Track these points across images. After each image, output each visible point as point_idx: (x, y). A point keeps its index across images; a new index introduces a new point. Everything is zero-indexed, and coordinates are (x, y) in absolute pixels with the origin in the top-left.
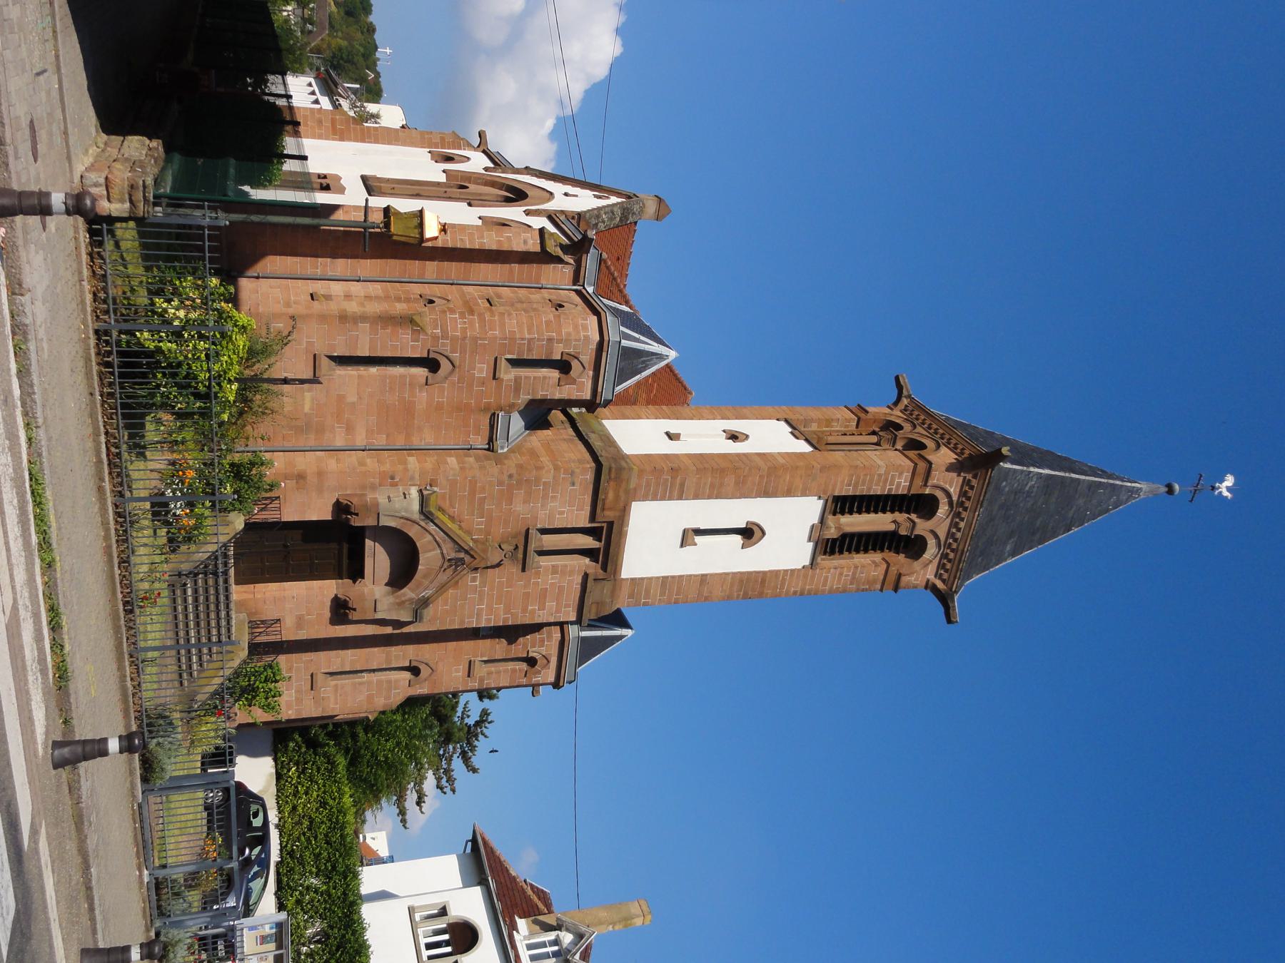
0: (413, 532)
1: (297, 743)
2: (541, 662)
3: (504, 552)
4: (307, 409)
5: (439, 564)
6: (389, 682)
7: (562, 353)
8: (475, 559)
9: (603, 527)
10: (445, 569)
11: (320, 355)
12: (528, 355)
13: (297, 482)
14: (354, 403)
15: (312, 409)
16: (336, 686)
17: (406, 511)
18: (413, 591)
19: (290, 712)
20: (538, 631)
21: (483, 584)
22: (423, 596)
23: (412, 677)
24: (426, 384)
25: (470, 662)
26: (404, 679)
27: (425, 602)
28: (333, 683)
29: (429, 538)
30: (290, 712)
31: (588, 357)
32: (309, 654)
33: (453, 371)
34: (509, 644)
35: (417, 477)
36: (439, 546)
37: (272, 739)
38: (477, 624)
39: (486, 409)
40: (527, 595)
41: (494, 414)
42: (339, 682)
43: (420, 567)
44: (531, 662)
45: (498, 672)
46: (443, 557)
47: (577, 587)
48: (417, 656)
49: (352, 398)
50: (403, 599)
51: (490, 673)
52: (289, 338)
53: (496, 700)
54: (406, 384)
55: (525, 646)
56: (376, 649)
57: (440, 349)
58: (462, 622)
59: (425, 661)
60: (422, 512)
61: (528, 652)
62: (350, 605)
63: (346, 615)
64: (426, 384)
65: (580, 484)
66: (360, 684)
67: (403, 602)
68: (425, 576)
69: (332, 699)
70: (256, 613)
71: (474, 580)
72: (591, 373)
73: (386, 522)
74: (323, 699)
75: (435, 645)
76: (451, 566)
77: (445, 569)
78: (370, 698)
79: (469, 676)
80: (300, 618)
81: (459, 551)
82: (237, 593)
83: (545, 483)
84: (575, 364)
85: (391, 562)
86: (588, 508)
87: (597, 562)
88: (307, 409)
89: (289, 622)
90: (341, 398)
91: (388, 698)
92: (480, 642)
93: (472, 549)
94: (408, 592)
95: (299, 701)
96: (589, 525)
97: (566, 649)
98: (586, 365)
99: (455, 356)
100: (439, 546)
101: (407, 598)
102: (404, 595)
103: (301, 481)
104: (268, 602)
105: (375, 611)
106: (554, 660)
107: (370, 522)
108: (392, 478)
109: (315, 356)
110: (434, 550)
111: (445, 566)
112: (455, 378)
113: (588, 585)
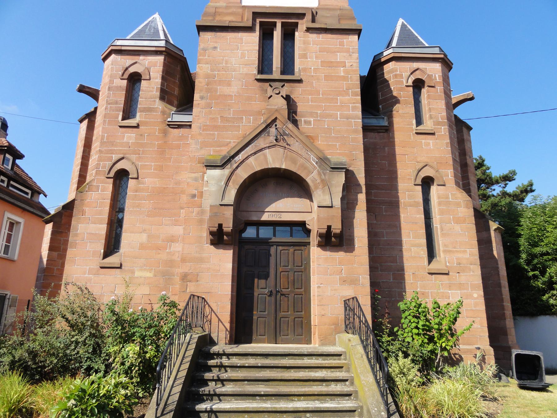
0: (243, 174)
1: (550, 297)
2: (418, 75)
3: (274, 95)
4: (149, 275)
5: (281, 150)
6: (440, 204)
7: (121, 79)
8: (276, 118)
9: (260, 22)
10: (287, 144)
11: (100, 263)
12: (120, 104)
13: (190, 281)
14: (149, 236)
15: (150, 271)
16: (444, 251)
17: (220, 180)
18: (310, 172)
19: (475, 295)
20: (388, 81)
21: (311, 114)
22: (316, 163)
23: (435, 184)
24: (137, 178)
25: (417, 133)
26: (437, 191)
27: (323, 160)
28: (442, 255)
29: (251, 159)
30: (475, 295)
31: (127, 60)
32: (406, 277)
33: (128, 159)
34: (399, 103)
35: (196, 175)
36: (261, 150)
37: (548, 317)
38: (359, 119)
39: (165, 133)
40: (328, 78)
41: (169, 125)
42: (441, 249)
43: (283, 167)
44: (418, 85)
45: (430, 110)
46: (274, 146)
47: (322, 37)
48: (410, 179)
49: (144, 238)
50: (319, 181)
51: (431, 117)
52: (84, 288)
53: (533, 181)
54: (136, 195)
55: (401, 89)
56: (402, 216)
57: (107, 170)
58: (355, 131)
59: (416, 172)
60: (222, 166)
61: (407, 86)
62: (324, 231)
63: (336, 235)
64: (137, 178)
65: (216, 42)
66: (442, 230)
67: (322, 181)
68: (294, 162)
69: (460, 255)
70: (336, 324)
71: (309, 123)
72: (141, 58)
73: (231, 196)
74: (460, 264)
75: (398, 165)
76: (284, 139)
77: (287, 144)
78: (458, 221)
79: (433, 134)
80: (344, 281)
81: (269, 133)
82: (315, 344)
83: (212, 70)
84: (132, 70)
85: (287, 197)
86: (240, 35)
87: (296, 24)
88: (149, 275)
89: (349, 293)
90: (142, 247)
91: (458, 205)
92: (396, 126)
93: (265, 121)
94: (312, 178)
95: (460, 286)
96: (257, 33)
97: (403, 55)
98: (134, 61)
99: (115, 157)
100: (261, 150)
101: (317, 177)
102: (314, 180)
103: (189, 278)
104: (323, 313)
105: (331, 207)
106: (415, 65)
107: (229, 213)
108: (194, 196)
109: (102, 268)
110: (265, 156)
111: (285, 145)
112: (134, 157)
113: (318, 27)
